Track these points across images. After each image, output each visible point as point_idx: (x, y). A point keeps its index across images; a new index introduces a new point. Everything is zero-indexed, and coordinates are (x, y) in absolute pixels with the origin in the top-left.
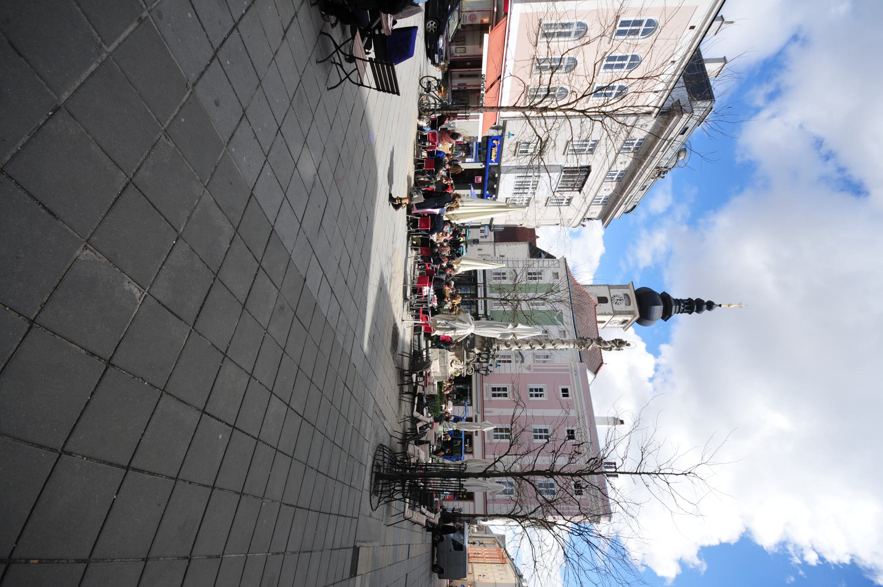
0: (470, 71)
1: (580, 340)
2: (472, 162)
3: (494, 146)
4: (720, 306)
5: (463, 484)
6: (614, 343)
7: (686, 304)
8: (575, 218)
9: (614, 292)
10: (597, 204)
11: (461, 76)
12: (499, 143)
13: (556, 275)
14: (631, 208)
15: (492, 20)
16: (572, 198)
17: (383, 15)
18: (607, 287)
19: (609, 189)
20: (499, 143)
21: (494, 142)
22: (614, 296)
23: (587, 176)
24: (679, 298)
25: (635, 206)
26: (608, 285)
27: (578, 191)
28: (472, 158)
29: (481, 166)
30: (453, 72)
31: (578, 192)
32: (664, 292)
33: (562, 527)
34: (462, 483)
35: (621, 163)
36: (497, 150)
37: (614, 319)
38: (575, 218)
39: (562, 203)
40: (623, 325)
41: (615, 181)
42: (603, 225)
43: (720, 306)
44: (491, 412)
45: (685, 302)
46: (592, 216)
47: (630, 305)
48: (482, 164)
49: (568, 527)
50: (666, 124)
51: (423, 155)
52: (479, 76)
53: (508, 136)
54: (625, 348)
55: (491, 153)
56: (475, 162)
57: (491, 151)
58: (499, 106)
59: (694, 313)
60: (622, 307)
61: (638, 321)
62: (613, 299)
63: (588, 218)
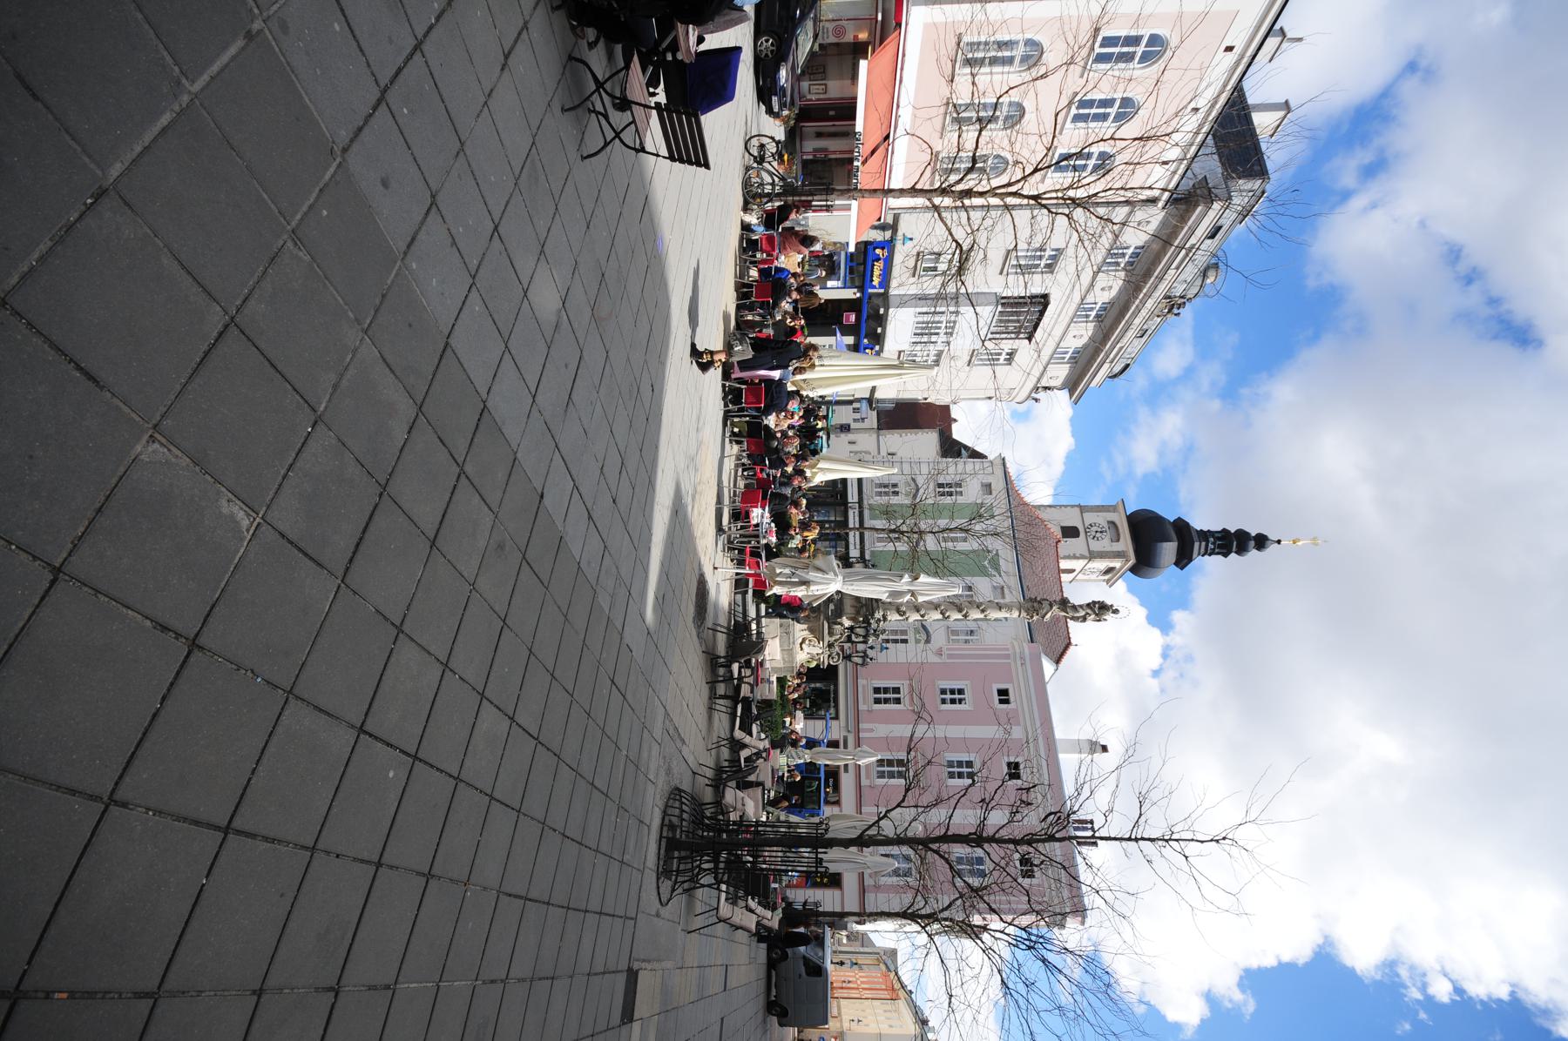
0: (834, 125)
1: (1030, 604)
2: (838, 288)
3: (878, 259)
4: (1279, 542)
5: (821, 859)
6: (1091, 608)
7: (1219, 539)
8: (1022, 387)
9: (1090, 518)
10: (1061, 361)
11: (819, 135)
12: (886, 254)
13: (988, 488)
14: (1120, 368)
15: (873, 36)
16: (1016, 350)
17: (680, 27)
18: (1077, 510)
19: (1082, 334)
20: (886, 254)
21: (878, 251)
22: (1091, 525)
23: (1042, 313)
24: (1205, 529)
25: (1127, 366)
26: (1080, 506)
27: (1026, 338)
28: (839, 280)
29: (855, 294)
30: (804, 129)
31: (1027, 341)
32: (1179, 518)
33: (998, 935)
34: (820, 856)
35: (1103, 289)
36: (882, 266)
37: (1090, 565)
38: (1022, 387)
39: (998, 359)
40: (1107, 577)
41: (1092, 322)
42: (1071, 398)
43: (1279, 542)
44: (871, 730)
45: (1217, 535)
46: (1052, 383)
47: (1118, 540)
48: (855, 290)
49: (1008, 935)
50: (1183, 219)
51: (751, 274)
52: (850, 134)
53: (901, 242)
54: (1109, 616)
55: (872, 271)
56: (844, 288)
57: (873, 268)
58: (886, 188)
59: (1233, 555)
60: (1104, 544)
61: (1134, 570)
62: (1088, 530)
63: (1043, 387)
